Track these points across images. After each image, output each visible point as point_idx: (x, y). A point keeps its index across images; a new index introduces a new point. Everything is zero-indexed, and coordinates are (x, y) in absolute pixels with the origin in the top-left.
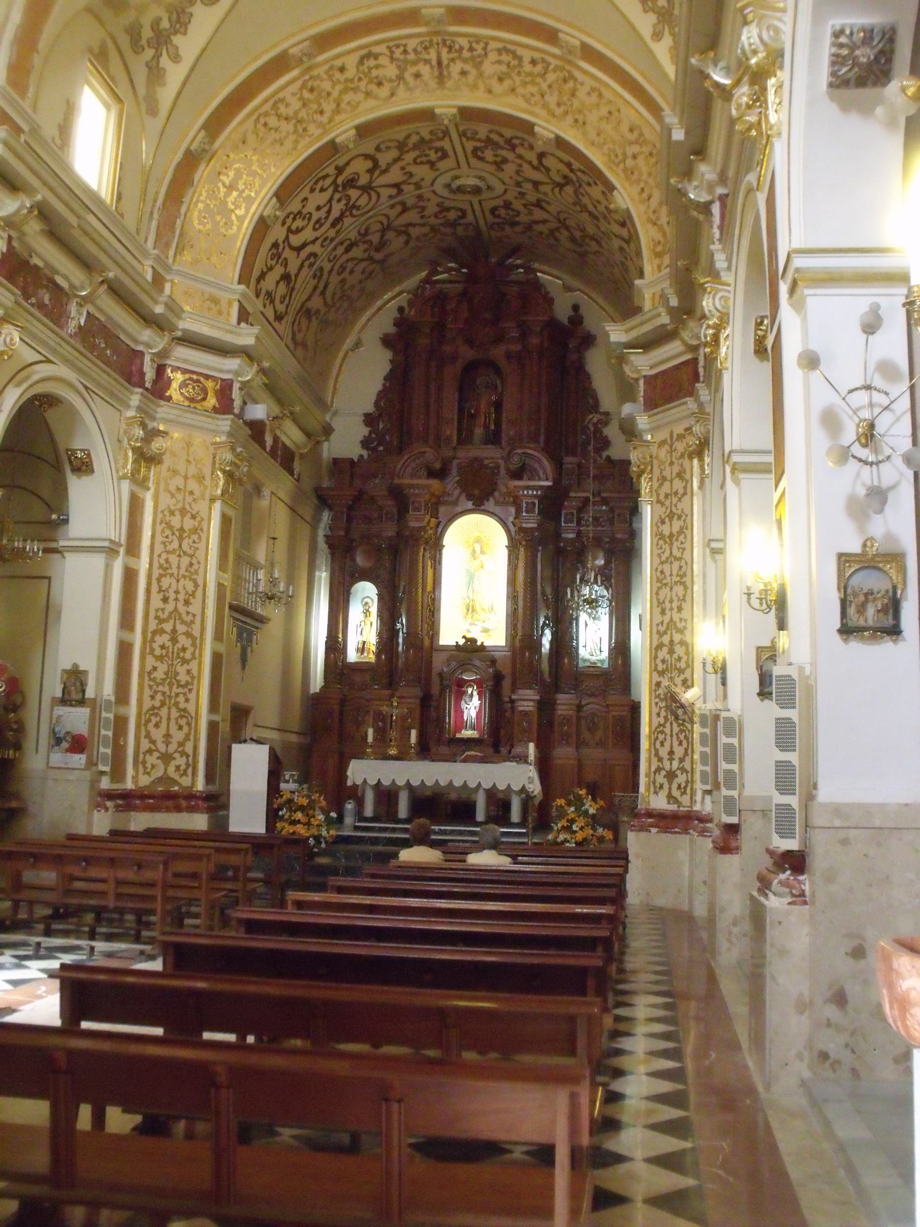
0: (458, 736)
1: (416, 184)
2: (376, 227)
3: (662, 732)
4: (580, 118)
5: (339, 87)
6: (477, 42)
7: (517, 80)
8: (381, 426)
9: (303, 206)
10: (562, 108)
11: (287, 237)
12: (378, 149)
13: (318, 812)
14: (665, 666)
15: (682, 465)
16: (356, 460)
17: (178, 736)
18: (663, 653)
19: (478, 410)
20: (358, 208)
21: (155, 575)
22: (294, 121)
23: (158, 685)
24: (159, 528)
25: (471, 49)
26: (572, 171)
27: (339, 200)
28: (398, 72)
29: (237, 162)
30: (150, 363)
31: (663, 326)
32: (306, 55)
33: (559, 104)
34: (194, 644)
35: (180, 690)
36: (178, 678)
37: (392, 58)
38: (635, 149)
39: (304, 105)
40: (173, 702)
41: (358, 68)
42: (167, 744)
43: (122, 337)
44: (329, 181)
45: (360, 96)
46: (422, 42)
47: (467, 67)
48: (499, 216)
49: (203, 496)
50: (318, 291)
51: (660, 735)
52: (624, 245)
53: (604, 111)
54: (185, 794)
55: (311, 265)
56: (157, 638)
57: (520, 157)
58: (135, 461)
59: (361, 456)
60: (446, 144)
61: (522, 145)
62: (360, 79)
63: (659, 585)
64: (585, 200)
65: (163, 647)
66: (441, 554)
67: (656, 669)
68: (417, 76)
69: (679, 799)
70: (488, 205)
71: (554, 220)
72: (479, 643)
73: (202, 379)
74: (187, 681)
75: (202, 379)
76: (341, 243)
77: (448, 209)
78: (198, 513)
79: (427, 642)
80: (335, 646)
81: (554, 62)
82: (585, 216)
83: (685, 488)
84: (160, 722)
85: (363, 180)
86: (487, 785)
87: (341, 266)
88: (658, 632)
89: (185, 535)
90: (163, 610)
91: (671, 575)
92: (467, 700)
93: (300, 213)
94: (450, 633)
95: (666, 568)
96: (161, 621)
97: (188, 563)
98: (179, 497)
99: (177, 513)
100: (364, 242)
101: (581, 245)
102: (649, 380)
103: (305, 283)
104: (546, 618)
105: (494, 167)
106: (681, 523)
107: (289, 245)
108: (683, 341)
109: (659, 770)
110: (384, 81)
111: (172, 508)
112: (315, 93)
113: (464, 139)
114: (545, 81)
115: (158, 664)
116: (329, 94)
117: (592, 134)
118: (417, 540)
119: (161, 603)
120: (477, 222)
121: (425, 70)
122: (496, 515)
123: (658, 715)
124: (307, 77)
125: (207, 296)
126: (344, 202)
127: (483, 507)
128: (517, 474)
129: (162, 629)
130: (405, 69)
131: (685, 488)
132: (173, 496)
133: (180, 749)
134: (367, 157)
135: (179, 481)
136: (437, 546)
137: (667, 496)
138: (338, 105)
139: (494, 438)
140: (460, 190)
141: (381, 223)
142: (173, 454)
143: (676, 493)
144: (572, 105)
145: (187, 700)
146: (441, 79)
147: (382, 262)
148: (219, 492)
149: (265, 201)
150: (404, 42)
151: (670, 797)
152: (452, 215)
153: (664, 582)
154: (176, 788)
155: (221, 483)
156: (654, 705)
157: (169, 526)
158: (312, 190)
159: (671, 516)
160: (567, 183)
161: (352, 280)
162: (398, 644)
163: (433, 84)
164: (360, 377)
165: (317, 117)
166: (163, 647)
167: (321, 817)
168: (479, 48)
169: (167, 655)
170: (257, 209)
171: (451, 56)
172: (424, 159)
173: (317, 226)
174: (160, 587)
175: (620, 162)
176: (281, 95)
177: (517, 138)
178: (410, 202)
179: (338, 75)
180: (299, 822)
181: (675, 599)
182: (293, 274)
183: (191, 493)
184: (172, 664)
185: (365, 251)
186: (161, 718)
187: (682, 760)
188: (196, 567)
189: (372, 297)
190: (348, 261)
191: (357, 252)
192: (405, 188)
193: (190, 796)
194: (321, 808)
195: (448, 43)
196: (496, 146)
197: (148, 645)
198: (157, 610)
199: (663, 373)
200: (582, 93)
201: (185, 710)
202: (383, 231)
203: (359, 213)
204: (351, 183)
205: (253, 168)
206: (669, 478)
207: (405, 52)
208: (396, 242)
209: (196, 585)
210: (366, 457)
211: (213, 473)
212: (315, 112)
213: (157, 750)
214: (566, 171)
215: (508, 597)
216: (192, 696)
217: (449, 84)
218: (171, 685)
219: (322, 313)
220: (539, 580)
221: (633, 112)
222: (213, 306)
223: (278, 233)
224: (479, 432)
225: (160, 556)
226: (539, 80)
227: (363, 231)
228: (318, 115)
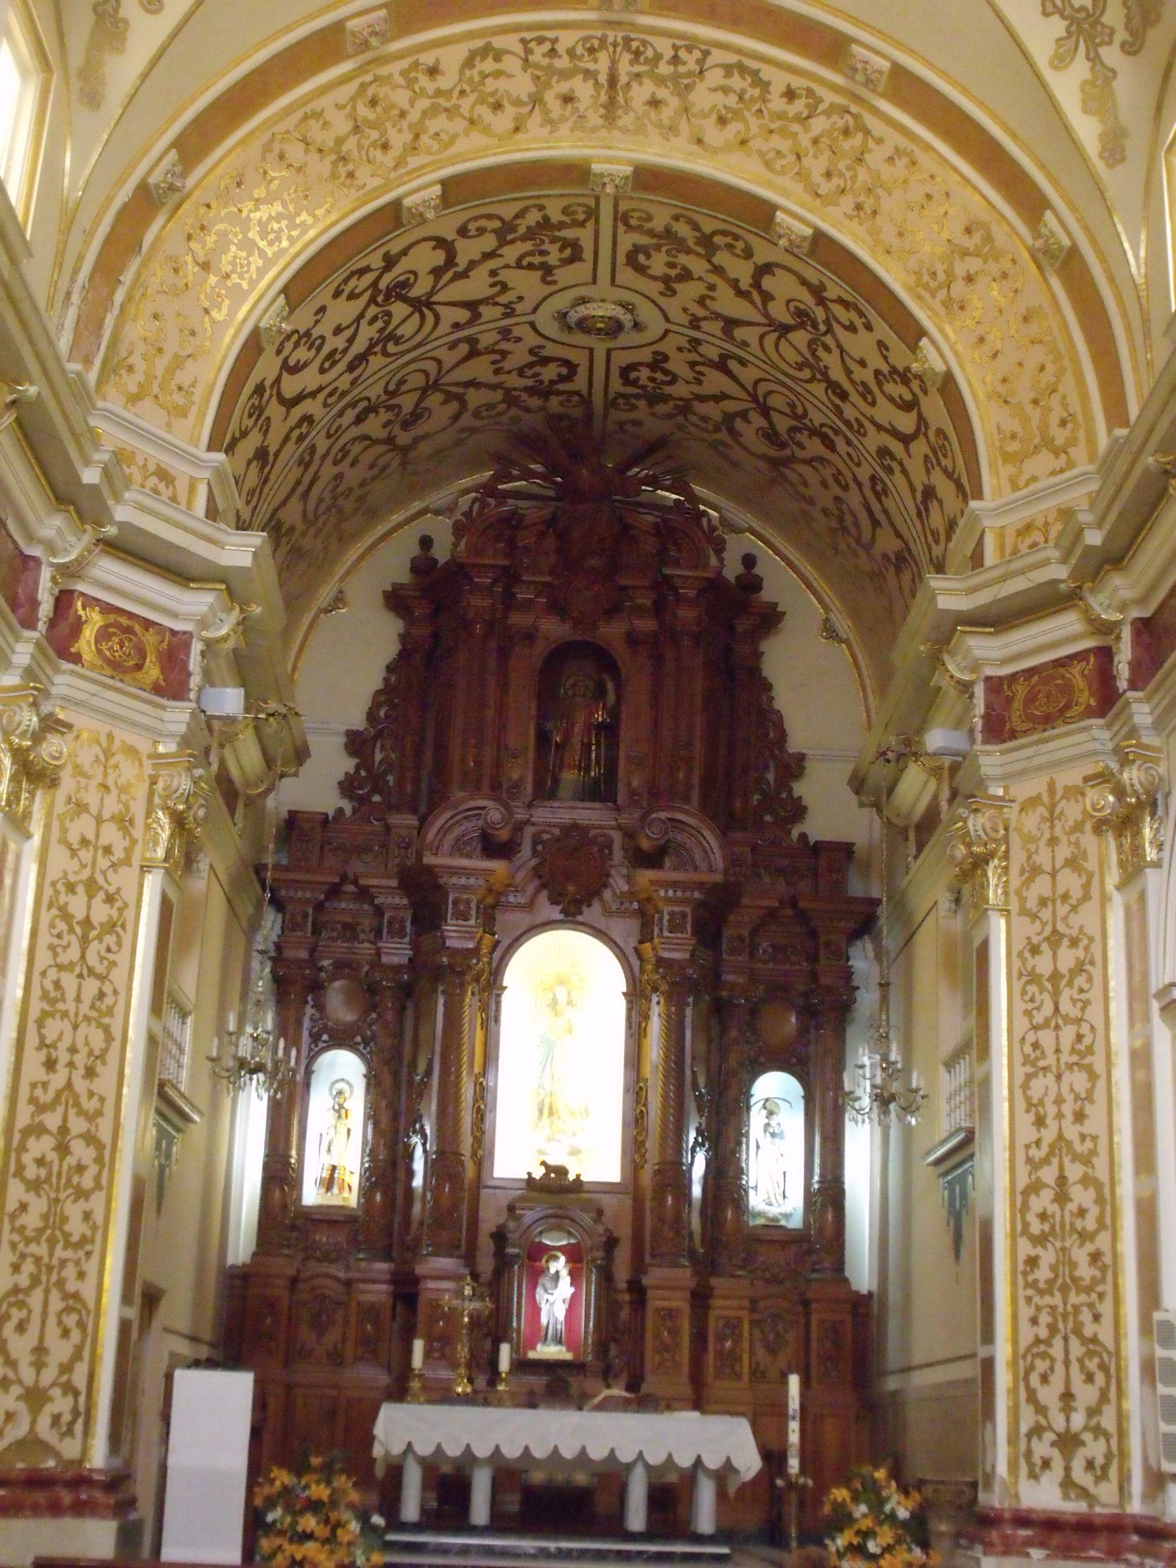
0: (531, 1355)
1: (506, 306)
2: (417, 381)
3: (1044, 1355)
4: (869, 204)
5: (423, 103)
6: (689, 49)
7: (754, 123)
8: (378, 756)
9: (317, 322)
10: (836, 182)
11: (278, 381)
12: (463, 232)
13: (346, 1515)
14: (1046, 1227)
15: (1077, 844)
16: (331, 814)
17: (60, 1351)
18: (1043, 1201)
19: (567, 736)
20: (397, 340)
21: (34, 1013)
22: (333, 157)
23: (28, 1241)
24: (45, 917)
25: (675, 60)
26: (821, 301)
27: (374, 319)
28: (533, 89)
29: (222, 221)
30: (49, 584)
31: (1054, 583)
32: (374, 33)
33: (828, 175)
34: (99, 1160)
35: (69, 1254)
36: (67, 1228)
37: (526, 60)
38: (973, 264)
39: (357, 129)
40: (54, 1277)
41: (461, 73)
42: (39, 1366)
43: (11, 525)
44: (369, 278)
45: (459, 125)
46: (586, 39)
47: (662, 93)
48: (634, 383)
49: (127, 861)
50: (300, 490)
51: (1038, 1362)
52: (896, 447)
53: (917, 193)
54: (69, 1474)
55: (301, 438)
56: (31, 1142)
57: (718, 270)
58: (14, 778)
59: (340, 811)
60: (584, 236)
61: (730, 247)
62: (462, 93)
63: (1029, 1069)
64: (831, 361)
65: (40, 1162)
66: (498, 1004)
67: (1025, 1231)
68: (568, 99)
69: (1092, 1490)
70: (621, 359)
71: (742, 394)
72: (571, 1177)
73: (138, 628)
74: (84, 1236)
75: (138, 628)
76: (353, 405)
77: (545, 361)
78: (119, 890)
79: (470, 1171)
80: (280, 1172)
81: (829, 97)
82: (819, 389)
83: (1086, 887)
84: (28, 1319)
85: (419, 290)
86: (424, 1449)
87: (343, 449)
88: (1029, 1160)
89: (93, 934)
90: (45, 1085)
91: (1058, 1051)
92: (548, 1284)
93: (308, 334)
94: (514, 1158)
95: (1046, 1038)
96: (41, 1108)
97: (96, 992)
98: (86, 855)
99: (80, 889)
100: (389, 408)
101: (782, 445)
102: (994, 685)
103: (285, 471)
104: (699, 1132)
105: (660, 286)
106: (1080, 953)
107: (279, 394)
108: (1087, 613)
109: (1037, 1431)
110: (505, 103)
111: (72, 878)
112: (379, 109)
113: (621, 228)
114: (807, 131)
115: (30, 1198)
116: (403, 114)
117: (889, 235)
118: (462, 974)
119: (43, 1070)
120: (590, 394)
121: (583, 90)
122: (522, 935)
123: (1034, 1321)
124: (368, 78)
125: (152, 468)
126: (379, 324)
127: (580, 918)
128: (652, 859)
129: (41, 1122)
130: (548, 86)
131: (1086, 887)
132: (74, 853)
133: (1093, 1422)
134: (441, 243)
135: (83, 826)
136: (492, 985)
137: (1043, 902)
138: (417, 137)
139: (600, 791)
140: (584, 325)
141: (426, 373)
142: (79, 771)
143: (1065, 897)
144: (854, 178)
145: (81, 1275)
146: (610, 110)
147: (405, 450)
148: (160, 853)
149: (263, 304)
150: (551, 34)
151: (1067, 1483)
152: (550, 372)
153: (1042, 1063)
154: (51, 1463)
155: (165, 835)
156: (1022, 1302)
157: (66, 916)
158: (337, 294)
159: (1055, 939)
160: (802, 325)
161: (353, 477)
162: (410, 1174)
163: (594, 118)
164: (348, 663)
165: (377, 154)
166: (40, 1162)
167: (354, 1526)
168: (690, 60)
169: (48, 1180)
170: (250, 312)
171: (637, 69)
172: (536, 260)
173: (327, 365)
174: (42, 1038)
175: (940, 287)
176: (317, 105)
177: (725, 233)
178: (486, 340)
179: (423, 80)
180: (308, 1536)
181: (1069, 1098)
182: (272, 450)
183: (108, 850)
184: (57, 1200)
185: (385, 425)
186: (30, 1312)
187: (1092, 1412)
188: (109, 1000)
189: (373, 515)
190: (355, 439)
191: (374, 426)
192: (487, 312)
193: (80, 1481)
194: (351, 1506)
195: (634, 44)
196: (680, 245)
197: (13, 1155)
198: (34, 1086)
199: (1030, 672)
200: (876, 157)
201: (76, 1296)
202: (425, 391)
203: (401, 348)
204: (399, 291)
205: (250, 235)
206: (1047, 867)
207: (553, 52)
208: (439, 411)
209: (109, 1038)
210: (348, 811)
211: (148, 814)
212: (374, 144)
213: (20, 1382)
214: (808, 299)
215: (627, 1090)
216: (91, 1267)
217: (625, 120)
218: (52, 1242)
219: (298, 532)
220: (688, 1060)
221: (977, 198)
222: (162, 487)
223: (266, 368)
224: (569, 777)
225: (44, 974)
226: (795, 127)
227: (392, 387)
228: (379, 151)
